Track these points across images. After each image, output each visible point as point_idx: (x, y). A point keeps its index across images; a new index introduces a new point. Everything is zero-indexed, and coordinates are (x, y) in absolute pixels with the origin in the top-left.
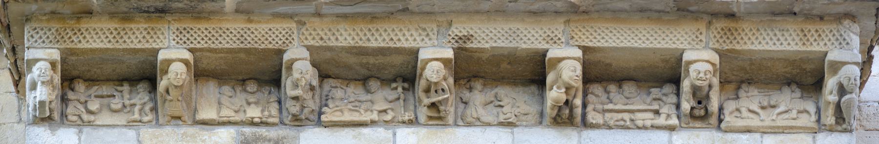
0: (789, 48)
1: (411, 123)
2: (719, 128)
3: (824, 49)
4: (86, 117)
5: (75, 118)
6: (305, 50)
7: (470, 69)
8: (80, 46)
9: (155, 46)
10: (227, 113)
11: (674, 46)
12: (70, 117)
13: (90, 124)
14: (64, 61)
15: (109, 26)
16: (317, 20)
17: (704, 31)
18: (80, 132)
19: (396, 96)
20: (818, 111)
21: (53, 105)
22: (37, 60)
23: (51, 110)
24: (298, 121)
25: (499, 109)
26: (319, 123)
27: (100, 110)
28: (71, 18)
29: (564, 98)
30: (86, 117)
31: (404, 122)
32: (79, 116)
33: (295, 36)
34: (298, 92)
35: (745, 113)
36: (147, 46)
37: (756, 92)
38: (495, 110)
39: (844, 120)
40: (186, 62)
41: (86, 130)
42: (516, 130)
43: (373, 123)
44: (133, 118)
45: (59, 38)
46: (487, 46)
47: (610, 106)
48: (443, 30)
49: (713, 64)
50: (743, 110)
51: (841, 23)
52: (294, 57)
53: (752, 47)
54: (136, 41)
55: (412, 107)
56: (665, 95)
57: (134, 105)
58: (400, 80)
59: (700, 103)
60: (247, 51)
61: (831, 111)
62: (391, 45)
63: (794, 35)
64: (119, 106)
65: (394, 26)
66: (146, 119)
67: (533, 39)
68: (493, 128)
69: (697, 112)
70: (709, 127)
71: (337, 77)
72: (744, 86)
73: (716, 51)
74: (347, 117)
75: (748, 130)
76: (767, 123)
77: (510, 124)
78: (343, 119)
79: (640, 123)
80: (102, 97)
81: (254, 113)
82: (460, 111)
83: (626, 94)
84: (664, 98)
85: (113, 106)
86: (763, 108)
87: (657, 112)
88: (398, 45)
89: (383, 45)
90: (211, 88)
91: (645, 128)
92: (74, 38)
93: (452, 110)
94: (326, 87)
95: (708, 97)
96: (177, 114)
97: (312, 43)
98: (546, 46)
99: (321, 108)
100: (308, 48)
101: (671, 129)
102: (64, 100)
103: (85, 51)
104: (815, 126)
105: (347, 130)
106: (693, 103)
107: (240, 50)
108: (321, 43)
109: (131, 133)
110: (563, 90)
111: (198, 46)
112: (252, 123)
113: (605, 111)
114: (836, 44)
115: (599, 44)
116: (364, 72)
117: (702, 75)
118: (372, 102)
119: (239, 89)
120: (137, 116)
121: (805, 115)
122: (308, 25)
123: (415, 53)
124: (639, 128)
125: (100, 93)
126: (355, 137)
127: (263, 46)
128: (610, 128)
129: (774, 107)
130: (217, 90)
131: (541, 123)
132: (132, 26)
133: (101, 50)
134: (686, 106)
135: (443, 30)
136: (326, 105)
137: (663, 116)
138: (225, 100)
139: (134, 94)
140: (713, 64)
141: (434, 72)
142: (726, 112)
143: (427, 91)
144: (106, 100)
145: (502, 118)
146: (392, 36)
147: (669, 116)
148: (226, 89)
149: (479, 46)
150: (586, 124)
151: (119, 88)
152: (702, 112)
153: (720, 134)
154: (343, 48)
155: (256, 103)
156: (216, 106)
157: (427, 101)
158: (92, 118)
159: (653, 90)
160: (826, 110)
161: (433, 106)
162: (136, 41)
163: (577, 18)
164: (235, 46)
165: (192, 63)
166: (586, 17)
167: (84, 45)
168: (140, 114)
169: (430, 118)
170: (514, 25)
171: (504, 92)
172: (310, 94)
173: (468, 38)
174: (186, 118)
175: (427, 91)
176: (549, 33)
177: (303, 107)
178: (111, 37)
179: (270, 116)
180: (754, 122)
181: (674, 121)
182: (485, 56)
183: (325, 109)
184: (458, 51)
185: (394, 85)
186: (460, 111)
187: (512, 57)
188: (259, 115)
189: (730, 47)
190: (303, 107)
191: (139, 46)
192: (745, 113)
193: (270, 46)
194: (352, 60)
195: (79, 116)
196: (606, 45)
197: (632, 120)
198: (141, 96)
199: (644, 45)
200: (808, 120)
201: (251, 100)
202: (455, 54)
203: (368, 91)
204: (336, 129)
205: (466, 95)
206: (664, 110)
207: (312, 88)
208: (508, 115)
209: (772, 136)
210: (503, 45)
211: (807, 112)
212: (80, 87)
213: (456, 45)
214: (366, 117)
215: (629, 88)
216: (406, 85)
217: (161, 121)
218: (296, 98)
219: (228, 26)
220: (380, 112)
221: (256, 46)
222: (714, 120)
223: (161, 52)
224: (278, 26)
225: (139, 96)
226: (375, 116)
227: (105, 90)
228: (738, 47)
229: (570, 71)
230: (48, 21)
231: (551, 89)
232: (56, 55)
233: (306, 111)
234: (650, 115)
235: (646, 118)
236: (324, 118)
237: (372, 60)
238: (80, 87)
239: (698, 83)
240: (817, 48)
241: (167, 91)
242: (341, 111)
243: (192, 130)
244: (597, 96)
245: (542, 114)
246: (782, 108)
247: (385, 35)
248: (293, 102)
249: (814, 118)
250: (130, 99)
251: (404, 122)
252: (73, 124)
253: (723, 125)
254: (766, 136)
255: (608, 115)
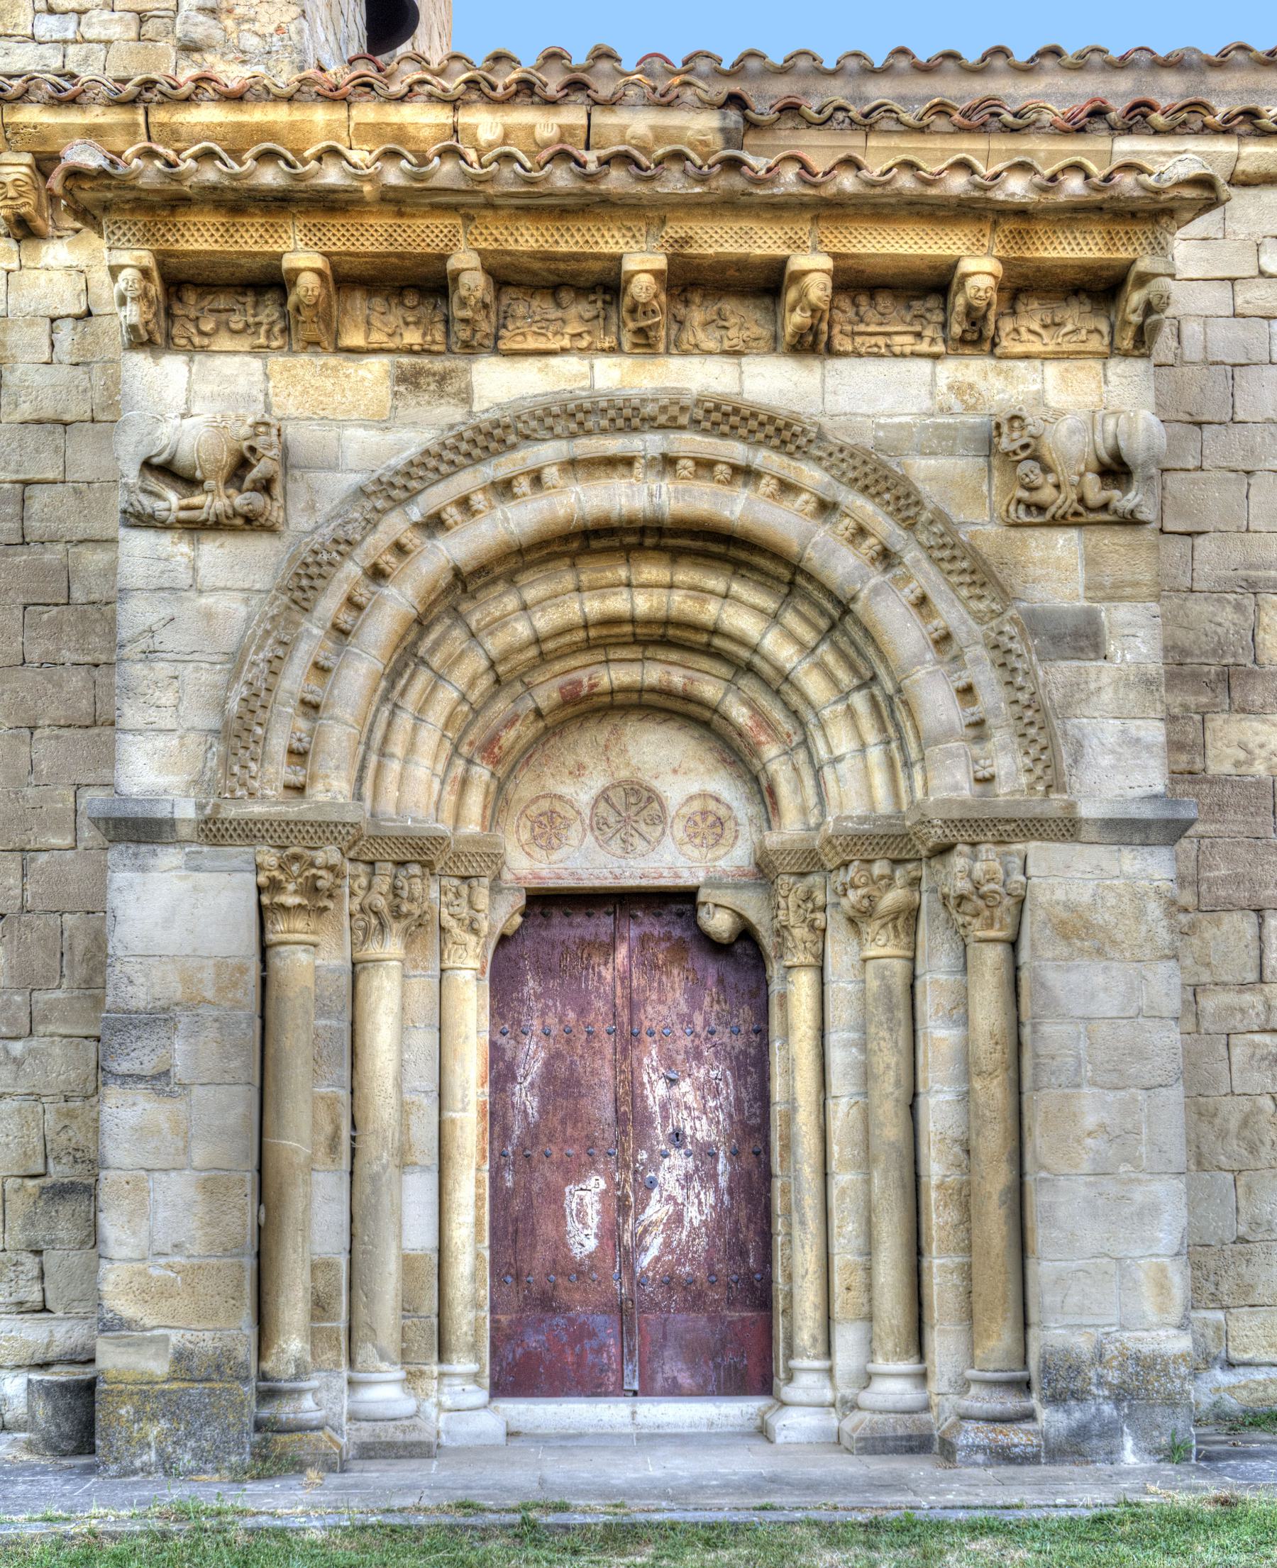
0: (1090, 255)
1: (612, 351)
2: (991, 353)
3: (1132, 256)
4: (197, 340)
5: (183, 342)
6: (475, 255)
7: (689, 281)
8: (177, 247)
9: (276, 248)
10: (378, 338)
11: (948, 252)
12: (177, 341)
13: (203, 349)
14: (161, 264)
15: (213, 220)
16: (489, 213)
17: (988, 232)
18: (191, 360)
19: (594, 313)
20: (1112, 333)
21: (151, 326)
22: (123, 267)
23: (149, 333)
24: (470, 349)
25: (723, 332)
26: (496, 351)
27: (216, 331)
28: (163, 207)
29: (809, 321)
30: (197, 340)
31: (603, 350)
32: (189, 339)
33: (461, 236)
34: (467, 313)
35: (1025, 335)
36: (266, 248)
37: (1035, 305)
38: (717, 334)
39: (1143, 343)
40: (319, 273)
41: (198, 358)
42: (744, 360)
43: (564, 351)
44: (258, 342)
45: (148, 236)
46: (711, 251)
47: (862, 328)
48: (653, 230)
49: (995, 277)
50: (1023, 330)
51: (1157, 222)
52: (460, 266)
53: (1045, 255)
54: (251, 242)
55: (614, 329)
56: (929, 310)
57: (259, 324)
58: (600, 290)
59: (973, 324)
60: (400, 256)
61: (1130, 333)
62: (587, 249)
63: (1098, 239)
64: (240, 326)
65: (590, 225)
66: (275, 344)
67: (770, 242)
68: (716, 358)
69: (969, 337)
70: (982, 354)
71: (518, 285)
72: (1021, 296)
73: (1000, 259)
74: (531, 343)
75: (1027, 357)
76: (1050, 348)
77: (735, 353)
78: (525, 346)
79: (897, 349)
80: (219, 311)
81: (412, 337)
82: (673, 332)
83: (880, 308)
84: (928, 315)
85: (233, 326)
86: (1045, 327)
87: (919, 335)
88: (596, 250)
89: (575, 249)
90: (358, 303)
91: (903, 355)
92: (168, 236)
93: (663, 333)
94: (505, 300)
95: (985, 317)
96: (313, 339)
97: (484, 245)
98: (787, 252)
99: (498, 329)
100: (480, 252)
101: (936, 357)
102: (170, 315)
103: (185, 254)
104: (1106, 350)
105: (531, 360)
106: (966, 326)
107: (389, 254)
108: (496, 245)
109: (256, 364)
110: (809, 314)
111: (334, 249)
112: (410, 351)
113: (854, 334)
114: (1148, 249)
115: (854, 250)
116: (552, 278)
117: (981, 293)
118: (564, 321)
119: (394, 301)
120: (262, 341)
121: (1095, 337)
122: (477, 222)
123: (618, 259)
124: (895, 355)
125: (215, 305)
126: (540, 370)
127: (419, 250)
128: (860, 355)
129: (1058, 325)
130: (365, 304)
131: (775, 350)
132: (245, 220)
133: (206, 252)
134: (956, 329)
135: (653, 230)
136: (505, 326)
137: (927, 340)
138: (376, 321)
139: (261, 308)
140: (995, 277)
141: (642, 287)
142: (1002, 334)
143: (633, 311)
144: (224, 316)
145: (726, 345)
146: (588, 237)
147: (933, 340)
148: (378, 303)
149: (701, 251)
150: (831, 352)
151: (241, 299)
152: (975, 336)
153: (993, 362)
154: (524, 253)
155: (416, 323)
156: (363, 328)
157: (631, 325)
158: (206, 341)
159: (914, 303)
160: (1122, 329)
161: (641, 332)
162: (251, 242)
163: (828, 213)
164: (382, 249)
165: (328, 272)
166: (841, 211)
167: (183, 246)
168: (268, 338)
169: (636, 345)
170: (746, 224)
171: (728, 306)
172: (483, 313)
173: (687, 241)
174: (326, 344)
175: (633, 311)
176: (791, 234)
177: (474, 331)
178: (217, 235)
179: (434, 342)
180: (1036, 347)
181: (939, 348)
182: (706, 262)
183: (503, 332)
184: (671, 259)
185: (592, 298)
186: (673, 332)
187: (742, 264)
188: (420, 341)
189: (1018, 254)
190: (474, 331)
191: (256, 248)
192: (1025, 335)
193: (429, 250)
194: (537, 265)
195: (189, 339)
196: (863, 251)
197: (887, 346)
198: (269, 313)
199: (911, 251)
200: (1096, 344)
201: (410, 319)
202: (669, 264)
203: (559, 305)
204: (517, 359)
205: (681, 310)
206: (928, 332)
207: (486, 306)
208: (735, 342)
209: (1055, 363)
210: (731, 250)
211: (1098, 331)
212: (191, 297)
213: (671, 250)
214: (555, 344)
215: (884, 302)
216: (608, 298)
217: (295, 347)
218: (465, 321)
219: (372, 221)
220: (573, 336)
221: (410, 249)
222: (987, 346)
223: (286, 257)
224: (437, 222)
225: (267, 311)
226: (566, 343)
227: (222, 302)
228: (1028, 255)
229: (818, 288)
230: (132, 211)
231: (793, 310)
232: (147, 259)
233: (478, 336)
234: (909, 339)
235: (903, 342)
236: (502, 345)
237: (562, 266)
238: (191, 297)
239: (976, 303)
240: (1123, 254)
241: (298, 310)
242: (523, 334)
243: (333, 361)
244: (844, 312)
245: (775, 338)
246: (1069, 327)
247: (578, 237)
248: (462, 326)
249: (1106, 340)
250: (255, 316)
251: (603, 350)
252: (180, 350)
253: (998, 351)
254: (1047, 363)
255: (859, 340)
